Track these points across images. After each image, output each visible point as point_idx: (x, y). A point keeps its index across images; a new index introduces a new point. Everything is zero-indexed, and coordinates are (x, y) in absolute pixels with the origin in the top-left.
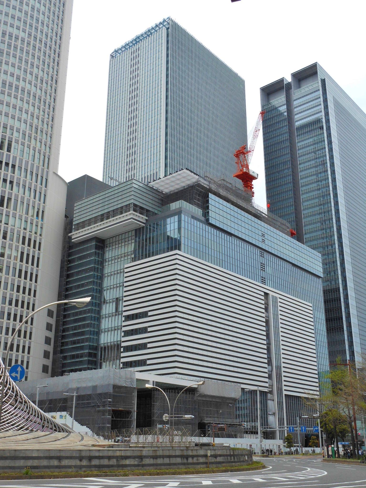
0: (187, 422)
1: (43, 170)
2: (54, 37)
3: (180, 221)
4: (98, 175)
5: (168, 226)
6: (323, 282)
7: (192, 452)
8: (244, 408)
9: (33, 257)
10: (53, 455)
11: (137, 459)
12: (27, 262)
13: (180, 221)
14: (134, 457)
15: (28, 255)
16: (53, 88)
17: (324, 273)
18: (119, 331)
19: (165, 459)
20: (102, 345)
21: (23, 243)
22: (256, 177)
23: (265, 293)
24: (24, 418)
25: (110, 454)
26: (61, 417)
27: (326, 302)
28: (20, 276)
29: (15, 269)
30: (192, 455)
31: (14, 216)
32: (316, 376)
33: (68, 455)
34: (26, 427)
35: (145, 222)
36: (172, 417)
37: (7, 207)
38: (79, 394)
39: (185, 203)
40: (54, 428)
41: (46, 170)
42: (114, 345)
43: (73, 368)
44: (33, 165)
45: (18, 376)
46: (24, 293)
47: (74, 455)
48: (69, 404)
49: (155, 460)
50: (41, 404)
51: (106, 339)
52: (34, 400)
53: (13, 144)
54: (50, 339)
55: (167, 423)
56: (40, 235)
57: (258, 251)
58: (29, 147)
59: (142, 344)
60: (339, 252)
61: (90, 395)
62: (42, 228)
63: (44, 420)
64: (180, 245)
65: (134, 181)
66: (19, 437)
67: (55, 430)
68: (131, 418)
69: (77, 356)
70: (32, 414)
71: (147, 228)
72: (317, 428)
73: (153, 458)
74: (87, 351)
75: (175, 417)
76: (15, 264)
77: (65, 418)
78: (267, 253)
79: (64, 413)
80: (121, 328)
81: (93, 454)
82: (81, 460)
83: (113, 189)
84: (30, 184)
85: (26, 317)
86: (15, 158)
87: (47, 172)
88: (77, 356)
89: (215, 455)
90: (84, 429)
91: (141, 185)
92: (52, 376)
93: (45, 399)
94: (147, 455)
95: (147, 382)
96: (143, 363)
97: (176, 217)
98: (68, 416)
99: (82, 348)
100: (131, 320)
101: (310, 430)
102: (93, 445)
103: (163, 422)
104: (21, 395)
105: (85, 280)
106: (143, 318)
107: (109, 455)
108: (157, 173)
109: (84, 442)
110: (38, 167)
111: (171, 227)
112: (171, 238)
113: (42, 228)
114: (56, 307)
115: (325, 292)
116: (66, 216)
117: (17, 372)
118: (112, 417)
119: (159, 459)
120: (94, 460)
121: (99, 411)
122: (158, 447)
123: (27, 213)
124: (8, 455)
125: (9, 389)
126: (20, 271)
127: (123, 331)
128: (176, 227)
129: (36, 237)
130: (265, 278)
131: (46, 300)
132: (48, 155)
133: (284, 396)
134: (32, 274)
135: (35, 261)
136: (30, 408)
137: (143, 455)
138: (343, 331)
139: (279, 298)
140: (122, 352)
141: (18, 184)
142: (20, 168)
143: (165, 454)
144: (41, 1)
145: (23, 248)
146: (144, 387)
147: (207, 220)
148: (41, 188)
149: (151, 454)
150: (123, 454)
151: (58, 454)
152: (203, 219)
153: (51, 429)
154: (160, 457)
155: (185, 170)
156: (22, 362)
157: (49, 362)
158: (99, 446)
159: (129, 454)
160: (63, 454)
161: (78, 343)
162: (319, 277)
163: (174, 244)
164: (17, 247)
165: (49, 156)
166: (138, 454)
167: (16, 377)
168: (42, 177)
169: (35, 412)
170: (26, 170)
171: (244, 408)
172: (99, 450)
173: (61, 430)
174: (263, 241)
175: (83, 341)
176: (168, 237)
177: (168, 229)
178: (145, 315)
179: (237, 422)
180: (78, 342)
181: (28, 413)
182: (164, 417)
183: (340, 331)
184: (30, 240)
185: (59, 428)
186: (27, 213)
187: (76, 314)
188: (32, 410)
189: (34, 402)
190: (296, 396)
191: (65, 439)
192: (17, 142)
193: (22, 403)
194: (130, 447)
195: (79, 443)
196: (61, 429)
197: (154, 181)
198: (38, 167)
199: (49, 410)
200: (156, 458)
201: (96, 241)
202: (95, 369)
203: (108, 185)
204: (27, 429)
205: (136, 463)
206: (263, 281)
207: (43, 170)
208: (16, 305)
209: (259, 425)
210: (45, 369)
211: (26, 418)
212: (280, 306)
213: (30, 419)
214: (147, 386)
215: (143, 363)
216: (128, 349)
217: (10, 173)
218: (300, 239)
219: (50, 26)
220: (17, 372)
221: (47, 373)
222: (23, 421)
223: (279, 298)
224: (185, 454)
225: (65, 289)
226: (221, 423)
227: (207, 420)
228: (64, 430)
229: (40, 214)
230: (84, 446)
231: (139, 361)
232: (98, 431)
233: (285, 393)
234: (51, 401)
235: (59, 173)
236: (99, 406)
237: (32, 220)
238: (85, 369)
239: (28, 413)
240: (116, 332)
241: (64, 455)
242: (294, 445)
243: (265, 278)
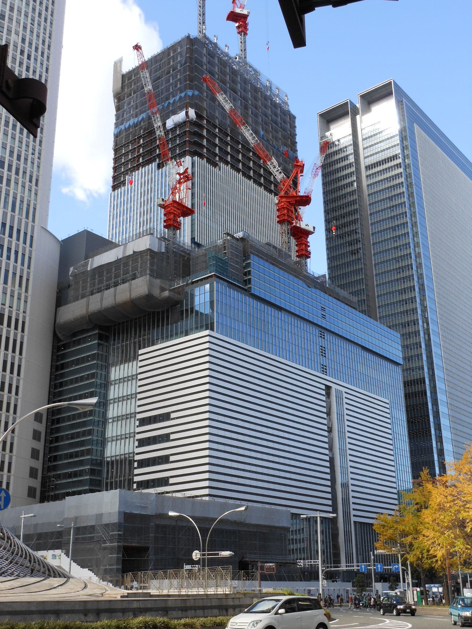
0: (224, 562)
1: (27, 224)
2: (40, 46)
6: (403, 371)
7: (233, 602)
8: (300, 540)
9: (15, 341)
10: (50, 609)
11: (160, 612)
17: (404, 358)
18: (132, 439)
19: (198, 611)
20: (109, 459)
22: (312, 230)
23: (326, 386)
25: (125, 606)
26: (54, 556)
27: (407, 396)
30: (232, 605)
32: (396, 496)
33: (69, 608)
34: (10, 571)
36: (204, 555)
38: (78, 526)
41: (30, 224)
42: (125, 459)
43: (70, 490)
44: (13, 217)
47: (77, 608)
48: (65, 538)
49: (184, 612)
50: (27, 539)
51: (112, 450)
52: (17, 534)
54: (38, 451)
55: (197, 562)
56: (24, 312)
57: (316, 331)
59: (163, 456)
60: (431, 389)
61: (93, 527)
62: (26, 302)
63: (35, 562)
68: (148, 557)
69: (75, 474)
70: (17, 554)
72: (397, 566)
73: (182, 611)
74: (89, 467)
75: (208, 555)
77: (60, 559)
78: (328, 333)
79: (58, 552)
80: (135, 436)
82: (86, 615)
85: (13, 424)
87: (33, 227)
88: (75, 474)
89: (166, 607)
90: (86, 574)
92: (42, 500)
93: (32, 533)
94: (173, 606)
98: (63, 556)
99: (81, 463)
100: (147, 425)
101: (388, 569)
103: (192, 562)
105: (86, 371)
106: (163, 421)
107: (124, 607)
109: (88, 591)
110: (20, 221)
112: (201, 314)
113: (26, 302)
115: (406, 384)
118: (123, 556)
119: (189, 612)
120: (103, 614)
121: (105, 548)
127: (137, 440)
128: (208, 299)
130: (326, 366)
133: (352, 523)
134: (12, 364)
136: (15, 546)
137: (168, 606)
138: (431, 435)
139: (345, 392)
140: (136, 468)
143: (197, 605)
144: (29, 2)
151: (56, 608)
157: (37, 483)
160: (62, 607)
161: (77, 456)
162: (397, 364)
165: (35, 205)
166: (162, 605)
168: (26, 234)
169: (22, 551)
171: (300, 540)
173: (52, 574)
174: (324, 316)
175: (82, 453)
176: (197, 312)
178: (166, 417)
179: (290, 560)
180: (77, 455)
181: (13, 553)
182: (194, 554)
183: (427, 436)
185: (54, 572)
187: (74, 417)
188: (18, 548)
189: (19, 537)
190: (366, 523)
196: (56, 573)
198: (20, 221)
199: (38, 548)
200: (186, 611)
202: (99, 491)
203: (115, 243)
204: (12, 574)
206: (324, 370)
207: (27, 224)
209: (320, 564)
210: (31, 492)
212: (346, 403)
213: (15, 561)
216: (143, 463)
218: (369, 312)
221: (34, 497)
222: (5, 563)
223: (345, 392)
224: (225, 604)
226: (269, 561)
227: (248, 558)
228: (61, 574)
230: (88, 595)
231: (158, 479)
232: (104, 575)
233: (353, 519)
234: (40, 536)
235: (48, 229)
236: (105, 542)
238: (85, 492)
239: (13, 553)
240: (127, 440)
241: (63, 608)
242: (368, 588)
243: (326, 366)
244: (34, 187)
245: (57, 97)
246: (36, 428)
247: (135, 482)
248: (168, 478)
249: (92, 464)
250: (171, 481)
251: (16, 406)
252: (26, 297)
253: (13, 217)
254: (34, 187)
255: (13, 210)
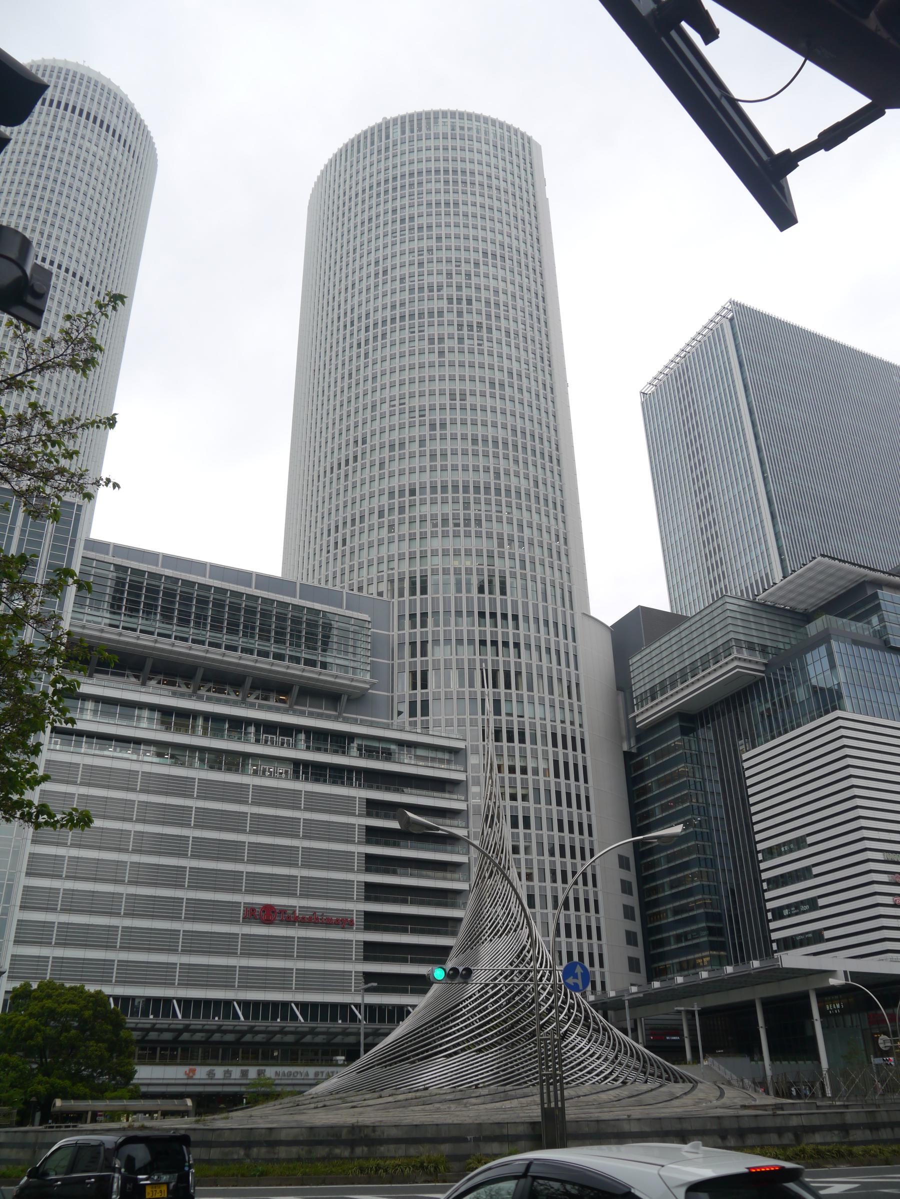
1: (564, 613)
3: (830, 655)
4: (661, 602)
5: (811, 668)
9: (576, 766)
11: (836, 1132)
12: (567, 777)
13: (830, 655)
14: (831, 1128)
15: (566, 764)
16: (556, 473)
21: (555, 745)
24: (606, 1060)
28: (559, 803)
29: (548, 792)
31: (531, 702)
35: (763, 668)
37: (517, 689)
39: (833, 619)
40: (665, 1075)
41: (568, 612)
44: (546, 609)
45: (579, 982)
46: (571, 831)
53: (508, 581)
56: (581, 726)
58: (534, 580)
62: (580, 713)
64: (840, 696)
65: (728, 600)
66: (604, 1096)
67: (668, 1079)
71: (769, 679)
73: (871, 1130)
76: (547, 783)
81: (746, 1124)
83: (693, 621)
84: (548, 641)
86: (515, 603)
87: (572, 616)
91: (742, 603)
95: (832, 973)
96: (817, 937)
97: (823, 649)
102: (744, 1107)
104: (594, 1018)
108: (767, 575)
110: (555, 611)
111: (817, 669)
112: (822, 689)
113: (580, 713)
114: (631, 846)
116: (619, 688)
117: (576, 977)
122: (878, 1106)
123: (551, 692)
124: (586, 1130)
125: (571, 1007)
126: (558, 794)
129: (573, 731)
131: (611, 840)
132: (568, 587)
135: (581, 773)
141: (528, 646)
142: (526, 618)
145: (556, 754)
146: (824, 985)
147: (886, 642)
148: (566, 645)
149: (863, 1119)
150: (805, 1121)
151: (677, 1126)
152: (876, 641)
153: (660, 1077)
154: (884, 1125)
155: (819, 558)
156: (581, 955)
158: (755, 1107)
159: (816, 1121)
160: (687, 1126)
163: (828, 700)
164: (545, 753)
166: (837, 1121)
167: (576, 985)
168: (565, 626)
170: (537, 620)
172: (756, 1116)
176: (814, 687)
177: (812, 674)
184: (564, 737)
186: (551, 692)
191: (689, 1096)
192: (513, 575)
193: (598, 1031)
194: (818, 1107)
195: (715, 1103)
197: (764, 590)
198: (555, 611)
201: (681, 720)
203: (682, 616)
205: (836, 1139)
207: (564, 613)
208: (563, 855)
211: (611, 1058)
214: (833, 982)
215: (817, 937)
217: (511, 630)
219: (532, 375)
220: (576, 977)
225: (640, 817)
229: (573, 690)
230: (729, 1107)
235: (593, 613)
237: (562, 703)
244: (560, 515)
245: (580, 533)
246: (624, 878)
247: (774, 941)
248: (808, 869)
249: (707, 920)
250: (827, 934)
251: (596, 902)
252: (580, 707)
253: (546, 609)
254: (560, 515)
255: (545, 599)
